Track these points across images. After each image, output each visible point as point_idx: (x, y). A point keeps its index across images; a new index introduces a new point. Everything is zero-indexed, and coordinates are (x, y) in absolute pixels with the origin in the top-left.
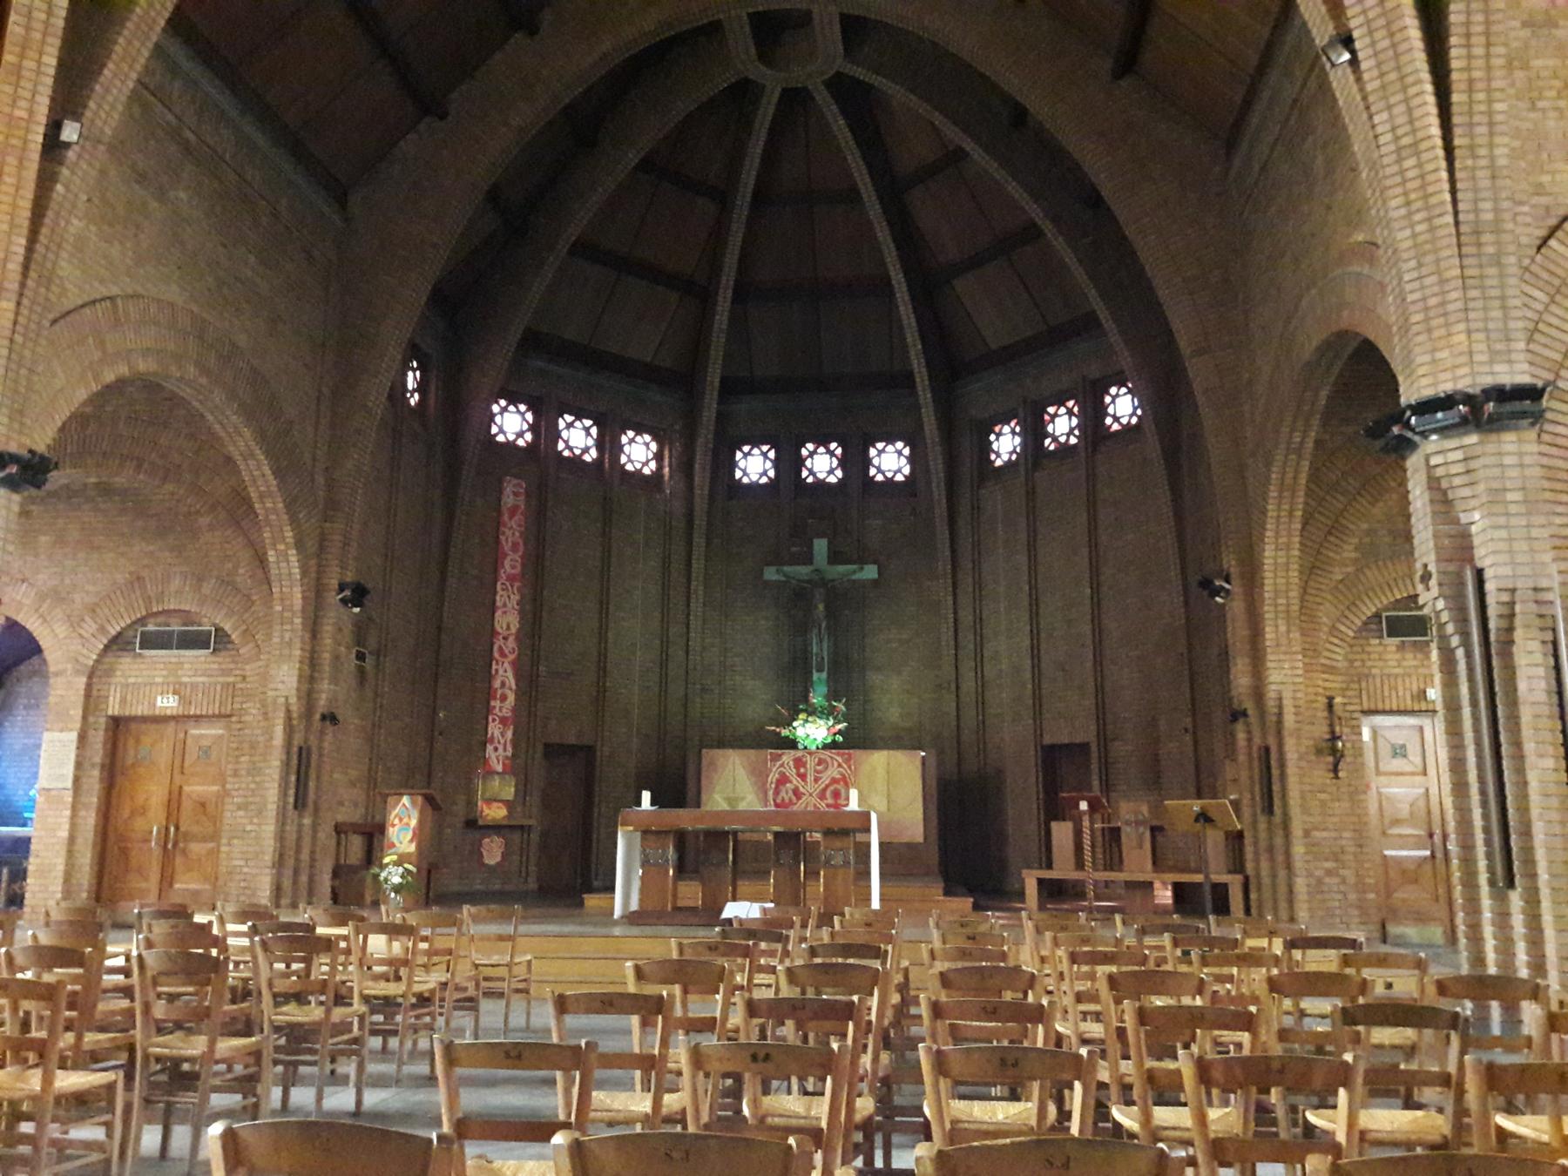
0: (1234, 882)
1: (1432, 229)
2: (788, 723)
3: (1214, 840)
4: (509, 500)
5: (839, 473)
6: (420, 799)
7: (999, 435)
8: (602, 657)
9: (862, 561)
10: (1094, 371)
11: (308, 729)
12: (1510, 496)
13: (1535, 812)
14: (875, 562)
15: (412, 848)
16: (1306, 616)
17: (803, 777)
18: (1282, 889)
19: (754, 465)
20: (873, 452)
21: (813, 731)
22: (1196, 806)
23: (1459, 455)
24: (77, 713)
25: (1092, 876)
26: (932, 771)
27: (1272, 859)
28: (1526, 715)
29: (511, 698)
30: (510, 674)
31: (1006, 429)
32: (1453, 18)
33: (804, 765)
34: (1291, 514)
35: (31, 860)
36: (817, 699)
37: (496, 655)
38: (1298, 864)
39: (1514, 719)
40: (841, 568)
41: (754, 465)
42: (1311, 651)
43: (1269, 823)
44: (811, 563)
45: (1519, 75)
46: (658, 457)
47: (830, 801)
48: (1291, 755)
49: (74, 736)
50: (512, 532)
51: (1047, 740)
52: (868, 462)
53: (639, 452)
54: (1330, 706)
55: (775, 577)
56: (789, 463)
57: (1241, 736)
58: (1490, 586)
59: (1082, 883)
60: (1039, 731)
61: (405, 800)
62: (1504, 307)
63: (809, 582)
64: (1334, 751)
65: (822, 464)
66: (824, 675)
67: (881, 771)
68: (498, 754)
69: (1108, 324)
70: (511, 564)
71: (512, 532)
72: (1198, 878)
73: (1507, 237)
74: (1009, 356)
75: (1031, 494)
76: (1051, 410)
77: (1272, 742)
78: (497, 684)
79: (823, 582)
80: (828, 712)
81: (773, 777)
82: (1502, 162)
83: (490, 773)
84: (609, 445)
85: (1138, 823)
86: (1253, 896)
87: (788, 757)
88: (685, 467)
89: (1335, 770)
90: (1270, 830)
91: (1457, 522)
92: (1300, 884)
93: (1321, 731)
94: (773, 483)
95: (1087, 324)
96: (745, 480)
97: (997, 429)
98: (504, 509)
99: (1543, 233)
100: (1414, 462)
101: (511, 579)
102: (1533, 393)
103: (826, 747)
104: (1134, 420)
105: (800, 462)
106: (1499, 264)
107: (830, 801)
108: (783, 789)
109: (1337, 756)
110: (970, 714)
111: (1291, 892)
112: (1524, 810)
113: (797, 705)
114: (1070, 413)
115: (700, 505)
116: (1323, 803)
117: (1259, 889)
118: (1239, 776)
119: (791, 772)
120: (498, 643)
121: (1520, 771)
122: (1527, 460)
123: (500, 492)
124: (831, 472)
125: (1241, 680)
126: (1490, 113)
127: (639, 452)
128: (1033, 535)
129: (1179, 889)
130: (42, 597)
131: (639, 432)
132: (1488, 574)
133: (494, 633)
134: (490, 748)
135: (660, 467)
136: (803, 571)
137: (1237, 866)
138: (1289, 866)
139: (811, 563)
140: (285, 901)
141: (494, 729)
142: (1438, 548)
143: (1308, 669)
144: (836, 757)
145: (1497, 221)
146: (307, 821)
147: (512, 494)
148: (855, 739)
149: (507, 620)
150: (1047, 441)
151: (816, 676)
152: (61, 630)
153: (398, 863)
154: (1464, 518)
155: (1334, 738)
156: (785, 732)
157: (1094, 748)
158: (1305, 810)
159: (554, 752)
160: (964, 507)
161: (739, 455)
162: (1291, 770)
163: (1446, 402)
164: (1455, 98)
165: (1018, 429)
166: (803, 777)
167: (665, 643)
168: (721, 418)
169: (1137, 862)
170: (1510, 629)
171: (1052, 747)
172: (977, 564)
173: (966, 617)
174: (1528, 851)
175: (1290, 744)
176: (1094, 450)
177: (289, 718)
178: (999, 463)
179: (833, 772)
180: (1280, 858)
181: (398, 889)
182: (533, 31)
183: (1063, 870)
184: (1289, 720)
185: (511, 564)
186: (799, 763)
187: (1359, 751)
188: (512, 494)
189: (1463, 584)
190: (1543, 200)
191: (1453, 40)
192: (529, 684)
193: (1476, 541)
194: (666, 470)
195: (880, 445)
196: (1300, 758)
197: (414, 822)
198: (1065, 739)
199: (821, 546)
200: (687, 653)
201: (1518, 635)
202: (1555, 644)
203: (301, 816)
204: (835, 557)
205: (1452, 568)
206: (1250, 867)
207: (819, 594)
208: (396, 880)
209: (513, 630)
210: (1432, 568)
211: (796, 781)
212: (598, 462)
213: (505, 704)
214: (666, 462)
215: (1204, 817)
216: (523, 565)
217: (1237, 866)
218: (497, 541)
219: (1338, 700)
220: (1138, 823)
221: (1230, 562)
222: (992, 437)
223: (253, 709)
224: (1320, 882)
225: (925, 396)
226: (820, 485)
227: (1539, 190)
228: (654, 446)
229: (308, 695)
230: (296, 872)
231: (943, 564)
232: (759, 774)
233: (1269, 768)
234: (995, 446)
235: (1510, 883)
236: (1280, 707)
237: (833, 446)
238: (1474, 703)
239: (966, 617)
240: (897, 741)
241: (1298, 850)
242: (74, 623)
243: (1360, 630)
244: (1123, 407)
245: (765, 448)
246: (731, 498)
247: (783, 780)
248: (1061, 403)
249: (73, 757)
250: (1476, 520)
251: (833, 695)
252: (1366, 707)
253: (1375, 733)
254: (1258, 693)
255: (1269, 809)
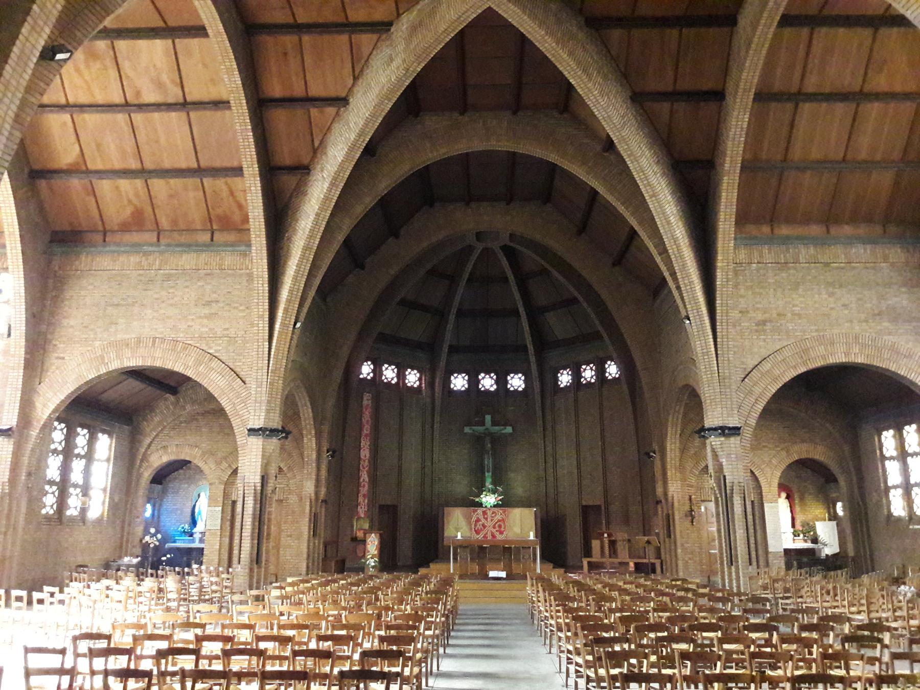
0: (657, 563)
1: (712, 377)
2: (479, 496)
3: (651, 552)
4: (365, 402)
5: (495, 387)
6: (378, 535)
7: (562, 374)
8: (400, 467)
9: (505, 425)
10: (601, 354)
11: (316, 505)
12: (733, 456)
13: (738, 544)
14: (511, 425)
15: (376, 552)
16: (681, 468)
17: (486, 519)
18: (674, 565)
19: (459, 382)
20: (509, 378)
21: (489, 499)
22: (646, 538)
23: (719, 443)
24: (221, 499)
25: (607, 560)
26: (539, 515)
27: (670, 555)
28: (736, 517)
29: (367, 486)
30: (366, 476)
31: (565, 372)
32: (718, 317)
33: (486, 514)
34: (676, 433)
35: (204, 557)
36: (489, 485)
37: (361, 468)
38: (679, 556)
39: (733, 522)
40: (497, 428)
41: (459, 382)
42: (684, 479)
43: (669, 541)
44: (484, 425)
45: (738, 328)
46: (420, 379)
47: (497, 529)
48: (677, 517)
49: (220, 508)
50: (367, 416)
51: (584, 503)
52: (506, 382)
53: (412, 378)
54: (690, 499)
55: (469, 431)
56: (474, 382)
57: (660, 509)
58: (727, 481)
59: (603, 563)
60: (580, 499)
61: (373, 535)
62: (731, 401)
63: (484, 433)
64: (692, 515)
65: (488, 382)
66: (490, 474)
67: (518, 516)
68: (362, 511)
69: (605, 335)
70: (367, 430)
71: (367, 416)
72: (645, 561)
73: (732, 381)
74: (568, 343)
75: (576, 401)
76: (584, 367)
77: (670, 512)
78: (361, 480)
79: (491, 435)
80: (494, 492)
81: (474, 519)
82: (731, 359)
83: (359, 518)
84: (401, 376)
85: (624, 541)
86: (664, 567)
87: (480, 511)
88: (431, 385)
89: (692, 522)
90: (670, 543)
91: (718, 461)
92: (680, 563)
93: (687, 508)
94: (467, 390)
95: (597, 336)
96: (455, 389)
97: (561, 371)
98: (364, 406)
99: (743, 376)
100: (708, 441)
101: (366, 435)
102: (738, 429)
103: (495, 506)
104: (617, 376)
105: (478, 381)
106: (730, 388)
107: (497, 529)
108: (478, 524)
109: (693, 517)
110: (551, 491)
111: (677, 566)
112: (736, 544)
113: (481, 489)
114: (591, 369)
115: (438, 403)
116: (688, 533)
117: (666, 564)
118: (658, 527)
119: (481, 517)
120: (362, 462)
121: (735, 533)
122: (737, 446)
123: (362, 398)
124: (492, 386)
125: (659, 490)
126: (728, 345)
127: (412, 378)
128: (577, 415)
129: (636, 564)
130: (204, 454)
131: (413, 369)
132: (727, 477)
133: (360, 458)
134: (359, 507)
135: (421, 384)
136: (480, 429)
137: (658, 556)
138: (676, 556)
139: (484, 425)
140: (310, 572)
141: (361, 499)
142: (714, 469)
143: (682, 485)
144: (499, 511)
145: (730, 376)
146: (317, 541)
147: (367, 400)
148: (505, 504)
149: (365, 453)
150: (582, 380)
151: (487, 474)
152: (213, 466)
153: (372, 558)
154: (721, 460)
155: (692, 510)
156: (477, 500)
157: (603, 508)
158: (682, 537)
159: (382, 507)
160: (548, 402)
161: (452, 378)
162: (677, 522)
163: (715, 429)
164: (718, 340)
165: (570, 373)
166: (486, 519)
167: (424, 461)
168: (448, 363)
169: (623, 554)
170: (732, 493)
171: (586, 506)
172: (553, 428)
173: (549, 449)
174: (737, 555)
175: (676, 513)
176: (602, 385)
177: (311, 502)
178: (562, 386)
179: (499, 517)
180: (673, 554)
181: (373, 567)
182: (397, 236)
183: (596, 557)
184: (676, 504)
185: (367, 430)
186: (484, 513)
187: (700, 515)
188: (367, 400)
189: (720, 480)
190: (744, 366)
191: (718, 324)
192: (374, 480)
193: (724, 467)
194: (423, 385)
195: (512, 375)
196: (680, 518)
197: (376, 543)
198: (591, 503)
199: (488, 418)
200: (432, 464)
201: (734, 495)
202: (744, 497)
203: (315, 539)
204: (494, 423)
205: (717, 474)
206: (663, 556)
207: (488, 439)
208: (373, 564)
209: (367, 457)
210: (712, 474)
211: (483, 521)
212: (398, 383)
213: (364, 490)
214: (423, 382)
215: (648, 542)
216: (371, 429)
217: (658, 556)
218: (361, 419)
219: (693, 497)
220: (624, 541)
221: (656, 447)
222: (559, 375)
223: (293, 499)
224: (687, 562)
225: (533, 359)
226: (487, 392)
227: (743, 363)
228: (418, 375)
229: (317, 493)
230: (313, 561)
231: (540, 429)
232: (468, 518)
233: (669, 521)
234: (560, 379)
235: (732, 564)
236: (673, 499)
237: (492, 375)
238: (723, 514)
239: (549, 449)
240: (525, 503)
241: (679, 551)
242: (218, 463)
243: (700, 472)
244: (612, 370)
245: (464, 375)
246: (449, 396)
247: (478, 520)
248: (588, 365)
249: (220, 516)
250: (724, 461)
251: (494, 483)
252: (703, 499)
253: (706, 508)
254: (666, 494)
255: (669, 536)
